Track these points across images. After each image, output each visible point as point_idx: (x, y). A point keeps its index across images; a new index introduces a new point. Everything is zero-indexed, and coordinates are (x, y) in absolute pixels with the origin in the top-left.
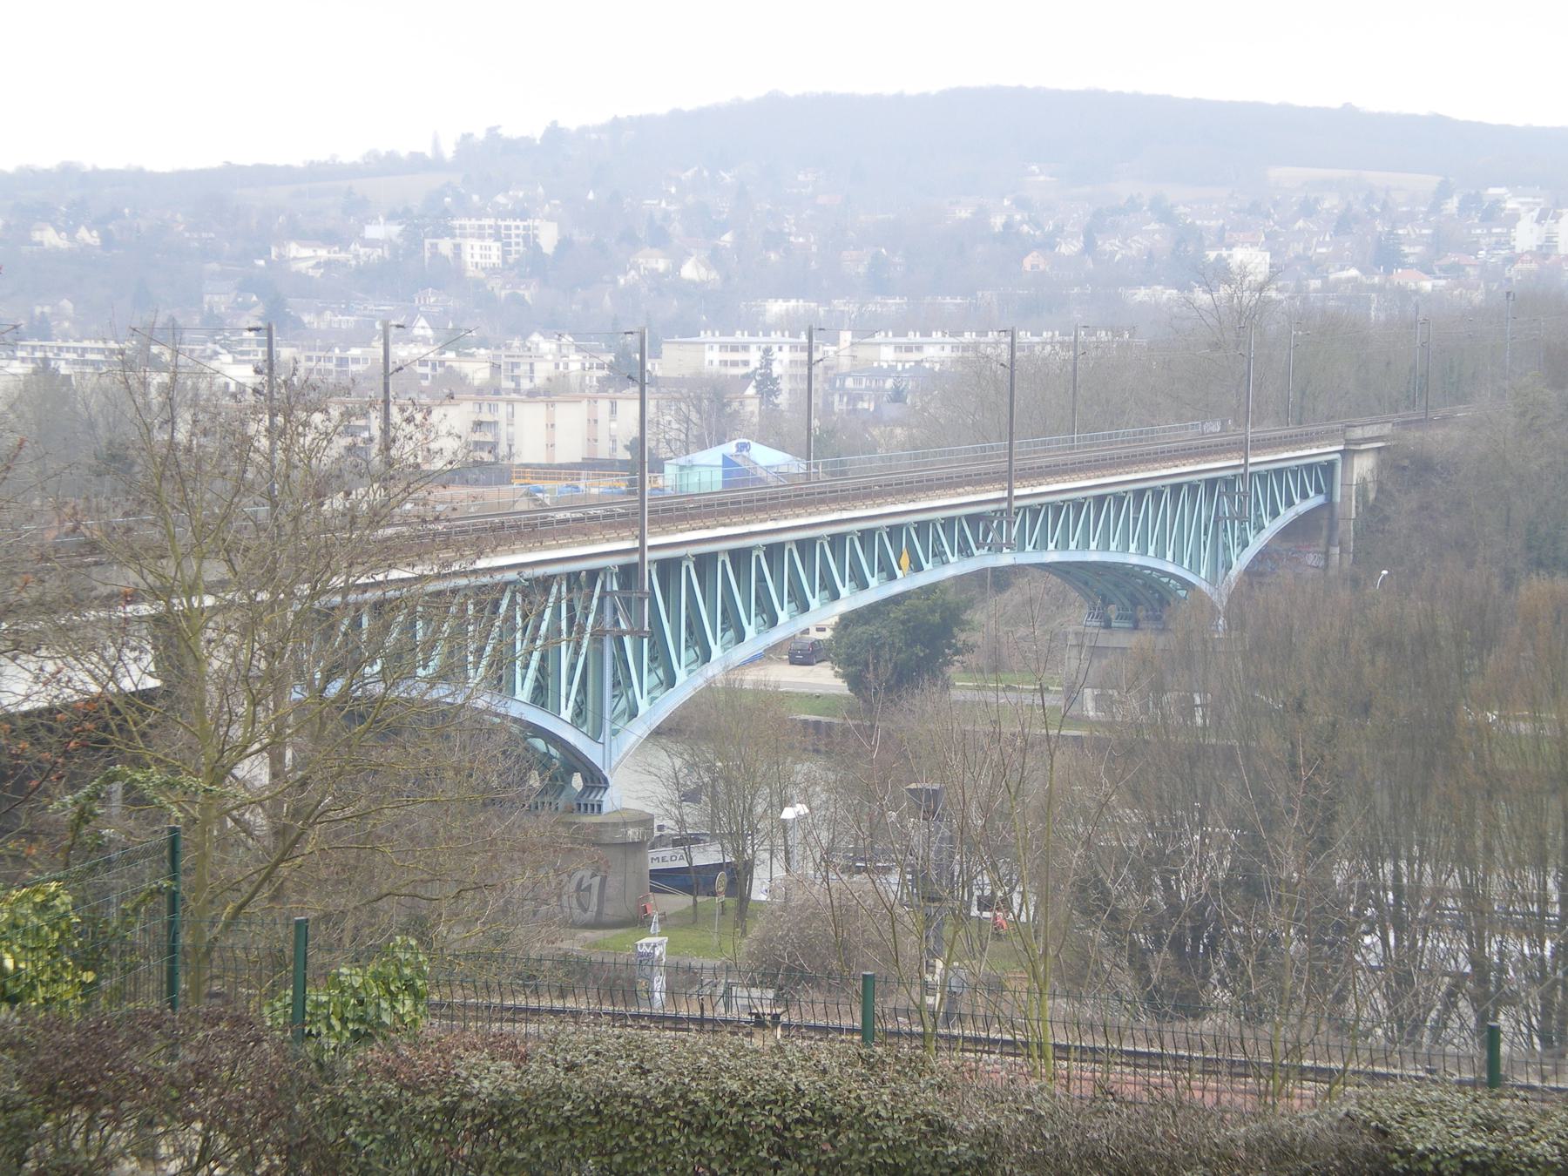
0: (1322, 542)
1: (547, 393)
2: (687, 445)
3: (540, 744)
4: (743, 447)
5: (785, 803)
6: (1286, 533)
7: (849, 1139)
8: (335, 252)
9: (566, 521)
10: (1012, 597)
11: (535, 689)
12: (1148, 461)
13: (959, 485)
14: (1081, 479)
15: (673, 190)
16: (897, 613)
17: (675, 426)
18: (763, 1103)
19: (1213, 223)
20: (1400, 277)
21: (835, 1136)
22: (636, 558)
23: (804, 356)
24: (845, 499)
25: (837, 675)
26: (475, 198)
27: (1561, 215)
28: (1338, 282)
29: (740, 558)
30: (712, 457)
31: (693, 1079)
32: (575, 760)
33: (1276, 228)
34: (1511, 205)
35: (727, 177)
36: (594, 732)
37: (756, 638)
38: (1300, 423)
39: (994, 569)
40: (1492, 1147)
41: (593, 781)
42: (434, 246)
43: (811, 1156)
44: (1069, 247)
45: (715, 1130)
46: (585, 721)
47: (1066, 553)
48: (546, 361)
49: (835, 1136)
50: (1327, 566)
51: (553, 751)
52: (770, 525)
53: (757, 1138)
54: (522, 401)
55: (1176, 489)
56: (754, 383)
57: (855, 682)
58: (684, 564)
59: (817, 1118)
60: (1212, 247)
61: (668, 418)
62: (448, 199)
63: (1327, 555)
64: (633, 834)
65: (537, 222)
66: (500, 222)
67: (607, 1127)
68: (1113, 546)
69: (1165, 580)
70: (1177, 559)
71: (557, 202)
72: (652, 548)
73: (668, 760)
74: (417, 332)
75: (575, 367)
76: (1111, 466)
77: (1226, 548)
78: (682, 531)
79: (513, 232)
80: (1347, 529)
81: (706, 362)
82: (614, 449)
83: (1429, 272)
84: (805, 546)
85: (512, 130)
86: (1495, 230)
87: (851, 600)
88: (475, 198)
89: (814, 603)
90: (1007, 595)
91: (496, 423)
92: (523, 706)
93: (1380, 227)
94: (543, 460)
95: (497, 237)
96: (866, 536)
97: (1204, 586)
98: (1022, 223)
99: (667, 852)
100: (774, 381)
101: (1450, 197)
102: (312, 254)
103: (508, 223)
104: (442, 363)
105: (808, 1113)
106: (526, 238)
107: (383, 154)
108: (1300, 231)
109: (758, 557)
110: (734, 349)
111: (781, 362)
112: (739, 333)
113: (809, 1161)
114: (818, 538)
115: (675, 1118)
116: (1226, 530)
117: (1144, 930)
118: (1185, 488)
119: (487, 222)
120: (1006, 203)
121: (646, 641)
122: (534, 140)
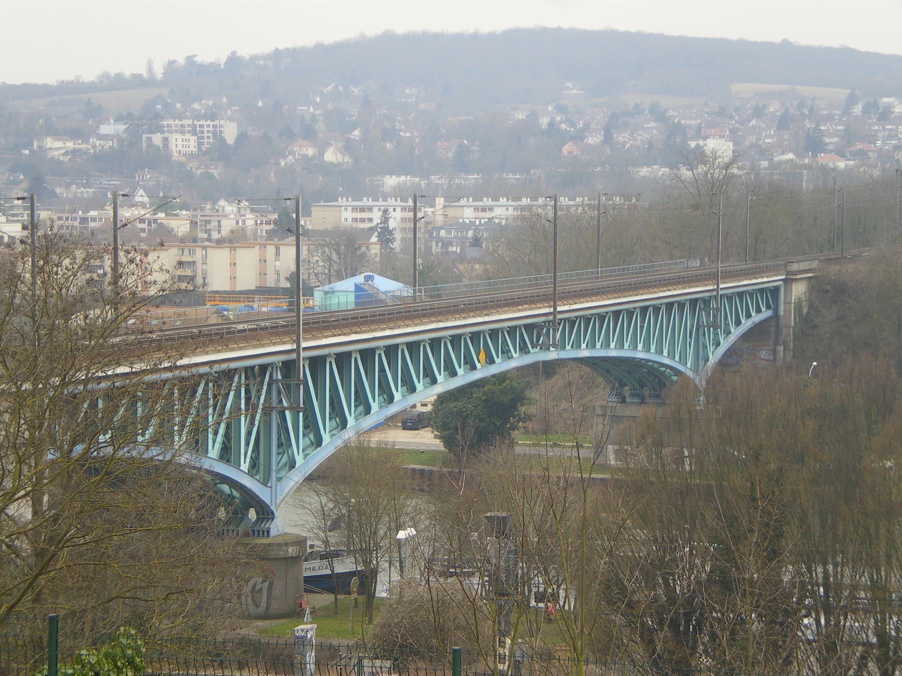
0: (771, 343)
1: (230, 241)
2: (330, 276)
3: (226, 488)
4: (368, 278)
5: (399, 527)
6: (746, 336)
8: (78, 144)
9: (244, 331)
10: (557, 382)
11: (222, 449)
12: (650, 287)
13: (519, 304)
15: (318, 100)
16: (477, 394)
17: (321, 264)
19: (693, 122)
20: (823, 158)
22: (294, 356)
23: (411, 214)
25: (436, 437)
26: (178, 105)
28: (781, 163)
29: (367, 355)
30: (347, 285)
32: (250, 499)
33: (737, 125)
35: (356, 91)
36: (264, 479)
37: (378, 412)
38: (755, 260)
41: (263, 514)
42: (149, 139)
51: (235, 492)
52: (388, 332)
56: (376, 234)
57: (449, 442)
60: (693, 139)
61: (317, 258)
62: (159, 107)
63: (775, 351)
64: (292, 551)
65: (222, 122)
66: (196, 122)
68: (626, 346)
69: (663, 369)
70: (671, 355)
71: (237, 108)
72: (305, 349)
73: (317, 498)
74: (138, 199)
75: (250, 223)
77: (705, 347)
78: (326, 337)
79: (206, 129)
80: (788, 333)
81: (343, 220)
82: (278, 280)
83: (843, 156)
84: (413, 347)
85: (205, 57)
86: (887, 127)
87: (445, 384)
88: (178, 105)
89: (419, 386)
90: (553, 380)
91: (194, 262)
93: (808, 124)
95: (194, 133)
96: (455, 340)
97: (690, 374)
98: (561, 122)
99: (316, 563)
100: (391, 232)
101: (857, 104)
102: (63, 146)
104: (155, 221)
106: (214, 133)
107: (113, 75)
109: (380, 355)
110: (362, 210)
117: (651, 616)
119: (186, 122)
121: (301, 414)
122: (141, 75)
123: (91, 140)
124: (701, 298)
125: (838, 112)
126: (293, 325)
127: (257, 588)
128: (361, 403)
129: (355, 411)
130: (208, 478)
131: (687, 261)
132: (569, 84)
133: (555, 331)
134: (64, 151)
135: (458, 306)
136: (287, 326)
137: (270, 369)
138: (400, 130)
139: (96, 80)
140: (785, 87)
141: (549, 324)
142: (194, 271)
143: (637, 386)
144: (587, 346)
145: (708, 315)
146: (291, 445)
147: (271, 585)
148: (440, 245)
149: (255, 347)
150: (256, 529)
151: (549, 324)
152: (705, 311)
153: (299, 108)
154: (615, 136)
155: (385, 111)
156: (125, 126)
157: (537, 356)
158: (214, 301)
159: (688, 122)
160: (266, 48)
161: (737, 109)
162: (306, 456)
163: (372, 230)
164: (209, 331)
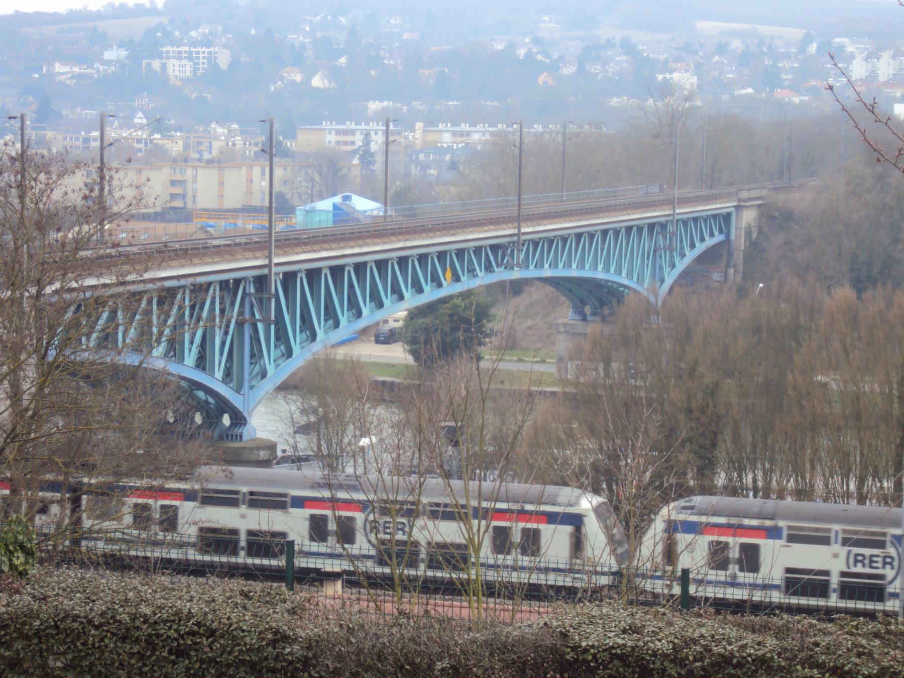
0: (723, 265)
1: (219, 161)
2: (312, 197)
3: (201, 394)
6: (700, 259)
8: (84, 69)
9: (219, 246)
10: (522, 300)
11: (198, 359)
12: (610, 211)
13: (484, 224)
15: (308, 28)
16: (445, 309)
17: (304, 184)
18: (165, 621)
19: (661, 57)
20: (779, 93)
21: (213, 642)
22: (265, 271)
23: (391, 138)
24: (408, 233)
26: (177, 33)
27: (881, 56)
28: (741, 96)
29: (337, 272)
30: (326, 205)
31: (122, 606)
32: (224, 406)
33: (701, 61)
34: (850, 49)
37: (347, 326)
38: (711, 187)
40: (630, 643)
41: (237, 420)
42: (149, 65)
43: (197, 655)
44: (568, 70)
45: (133, 639)
46: (231, 380)
49: (213, 642)
50: (726, 281)
51: (211, 400)
52: (357, 250)
53: (161, 644)
55: (629, 229)
56: (358, 156)
57: (415, 353)
58: (299, 275)
59: (202, 631)
61: (300, 179)
62: (159, 34)
63: (726, 274)
64: (263, 455)
65: (217, 49)
66: (192, 49)
68: (587, 266)
69: (621, 289)
70: (630, 275)
71: (231, 36)
72: (277, 265)
74: (137, 121)
77: (661, 268)
78: (297, 253)
79: (201, 55)
80: (739, 257)
81: (327, 142)
83: (798, 92)
84: (381, 265)
87: (412, 300)
88: (177, 33)
92: (190, 369)
95: (190, 58)
98: (538, 53)
100: (372, 155)
101: (812, 43)
102: (70, 70)
103: (197, 49)
105: (196, 628)
106: (209, 59)
107: (118, 4)
109: (349, 272)
110: (345, 133)
111: (377, 142)
112: (348, 123)
113: (195, 658)
114: (390, 259)
115: (107, 631)
116: (661, 257)
118: (635, 229)
120: (527, 40)
121: (273, 327)
122: (143, 5)
123: (96, 66)
124: (658, 223)
126: (265, 242)
128: (331, 318)
129: (324, 325)
130: (184, 384)
131: (648, 187)
132: (546, 18)
134: (70, 75)
136: (260, 242)
137: (243, 283)
138: (384, 58)
139: (102, 9)
140: (745, 26)
141: (514, 245)
143: (597, 304)
145: (665, 238)
146: (262, 356)
148: (419, 168)
149: (229, 261)
150: (230, 433)
151: (514, 245)
152: (662, 235)
153: (290, 36)
154: (588, 68)
155: (371, 40)
156: (127, 53)
157: (501, 275)
159: (656, 56)
161: (702, 45)
162: (277, 366)
163: (354, 152)
164: (186, 245)
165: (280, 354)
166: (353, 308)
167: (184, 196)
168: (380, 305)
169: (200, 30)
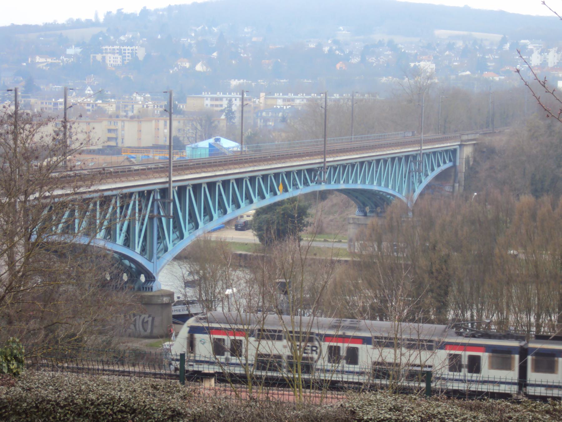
0: (452, 181)
1: (138, 117)
2: (196, 139)
3: (127, 262)
4: (217, 140)
7: (139, 418)
8: (54, 60)
9: (138, 170)
10: (327, 203)
11: (125, 240)
12: (381, 148)
13: (303, 156)
14: (354, 155)
15: (193, 35)
16: (279, 210)
17: (191, 131)
18: (104, 404)
19: (413, 52)
21: (134, 417)
22: (167, 185)
23: (245, 103)
25: (255, 235)
26: (112, 38)
28: (462, 76)
29: (211, 186)
30: (205, 144)
32: (141, 269)
33: (438, 54)
34: (530, 47)
35: (215, 29)
37: (218, 219)
38: (444, 133)
39: (320, 192)
40: (394, 417)
41: (149, 278)
42: (94, 57)
44: (355, 60)
46: (146, 253)
47: (348, 185)
48: (139, 104)
49: (134, 417)
51: (133, 266)
53: (102, 418)
54: (128, 121)
55: (393, 159)
56: (224, 114)
59: (127, 410)
60: (412, 62)
61: (188, 128)
62: (100, 38)
63: (453, 187)
64: (166, 300)
65: (137, 48)
66: (121, 48)
67: (40, 413)
68: (367, 182)
69: (388, 196)
70: (394, 188)
71: (145, 39)
72: (174, 181)
73: (180, 270)
74: (87, 92)
76: (367, 149)
77: (413, 183)
78: (187, 174)
79: (127, 51)
80: (461, 176)
81: (205, 105)
83: (498, 74)
84: (239, 181)
85: (127, 10)
87: (258, 203)
88: (112, 38)
90: (326, 202)
94: (136, 145)
95: (120, 53)
96: (265, 178)
97: (405, 200)
98: (336, 50)
99: (179, 307)
102: (45, 61)
105: (123, 408)
106: (132, 54)
107: (75, 20)
108: (447, 55)
109: (219, 186)
110: (217, 99)
111: (236, 105)
112: (218, 93)
115: (69, 410)
116: (413, 176)
119: (116, 47)
122: (91, 20)
123: (61, 58)
125: (495, 48)
126: (167, 167)
127: (146, 320)
129: (204, 219)
130: (116, 256)
131: (405, 133)
132: (341, 28)
133: (325, 173)
134: (46, 64)
135: (266, 157)
139: (65, 23)
140: (465, 33)
141: (321, 169)
142: (117, 134)
143: (374, 206)
144: (344, 182)
146: (165, 238)
147: (153, 319)
148: (262, 121)
149: (144, 179)
150: (145, 286)
151: (321, 169)
152: (414, 162)
153: (182, 39)
156: (81, 50)
157: (313, 187)
158: (127, 152)
159: (410, 51)
160: (163, 5)
161: (438, 45)
162: (174, 244)
163: (222, 111)
165: (176, 237)
166: (221, 208)
167: (116, 139)
168: (238, 206)
169: (126, 36)
